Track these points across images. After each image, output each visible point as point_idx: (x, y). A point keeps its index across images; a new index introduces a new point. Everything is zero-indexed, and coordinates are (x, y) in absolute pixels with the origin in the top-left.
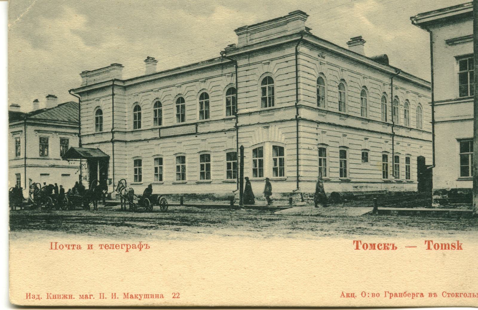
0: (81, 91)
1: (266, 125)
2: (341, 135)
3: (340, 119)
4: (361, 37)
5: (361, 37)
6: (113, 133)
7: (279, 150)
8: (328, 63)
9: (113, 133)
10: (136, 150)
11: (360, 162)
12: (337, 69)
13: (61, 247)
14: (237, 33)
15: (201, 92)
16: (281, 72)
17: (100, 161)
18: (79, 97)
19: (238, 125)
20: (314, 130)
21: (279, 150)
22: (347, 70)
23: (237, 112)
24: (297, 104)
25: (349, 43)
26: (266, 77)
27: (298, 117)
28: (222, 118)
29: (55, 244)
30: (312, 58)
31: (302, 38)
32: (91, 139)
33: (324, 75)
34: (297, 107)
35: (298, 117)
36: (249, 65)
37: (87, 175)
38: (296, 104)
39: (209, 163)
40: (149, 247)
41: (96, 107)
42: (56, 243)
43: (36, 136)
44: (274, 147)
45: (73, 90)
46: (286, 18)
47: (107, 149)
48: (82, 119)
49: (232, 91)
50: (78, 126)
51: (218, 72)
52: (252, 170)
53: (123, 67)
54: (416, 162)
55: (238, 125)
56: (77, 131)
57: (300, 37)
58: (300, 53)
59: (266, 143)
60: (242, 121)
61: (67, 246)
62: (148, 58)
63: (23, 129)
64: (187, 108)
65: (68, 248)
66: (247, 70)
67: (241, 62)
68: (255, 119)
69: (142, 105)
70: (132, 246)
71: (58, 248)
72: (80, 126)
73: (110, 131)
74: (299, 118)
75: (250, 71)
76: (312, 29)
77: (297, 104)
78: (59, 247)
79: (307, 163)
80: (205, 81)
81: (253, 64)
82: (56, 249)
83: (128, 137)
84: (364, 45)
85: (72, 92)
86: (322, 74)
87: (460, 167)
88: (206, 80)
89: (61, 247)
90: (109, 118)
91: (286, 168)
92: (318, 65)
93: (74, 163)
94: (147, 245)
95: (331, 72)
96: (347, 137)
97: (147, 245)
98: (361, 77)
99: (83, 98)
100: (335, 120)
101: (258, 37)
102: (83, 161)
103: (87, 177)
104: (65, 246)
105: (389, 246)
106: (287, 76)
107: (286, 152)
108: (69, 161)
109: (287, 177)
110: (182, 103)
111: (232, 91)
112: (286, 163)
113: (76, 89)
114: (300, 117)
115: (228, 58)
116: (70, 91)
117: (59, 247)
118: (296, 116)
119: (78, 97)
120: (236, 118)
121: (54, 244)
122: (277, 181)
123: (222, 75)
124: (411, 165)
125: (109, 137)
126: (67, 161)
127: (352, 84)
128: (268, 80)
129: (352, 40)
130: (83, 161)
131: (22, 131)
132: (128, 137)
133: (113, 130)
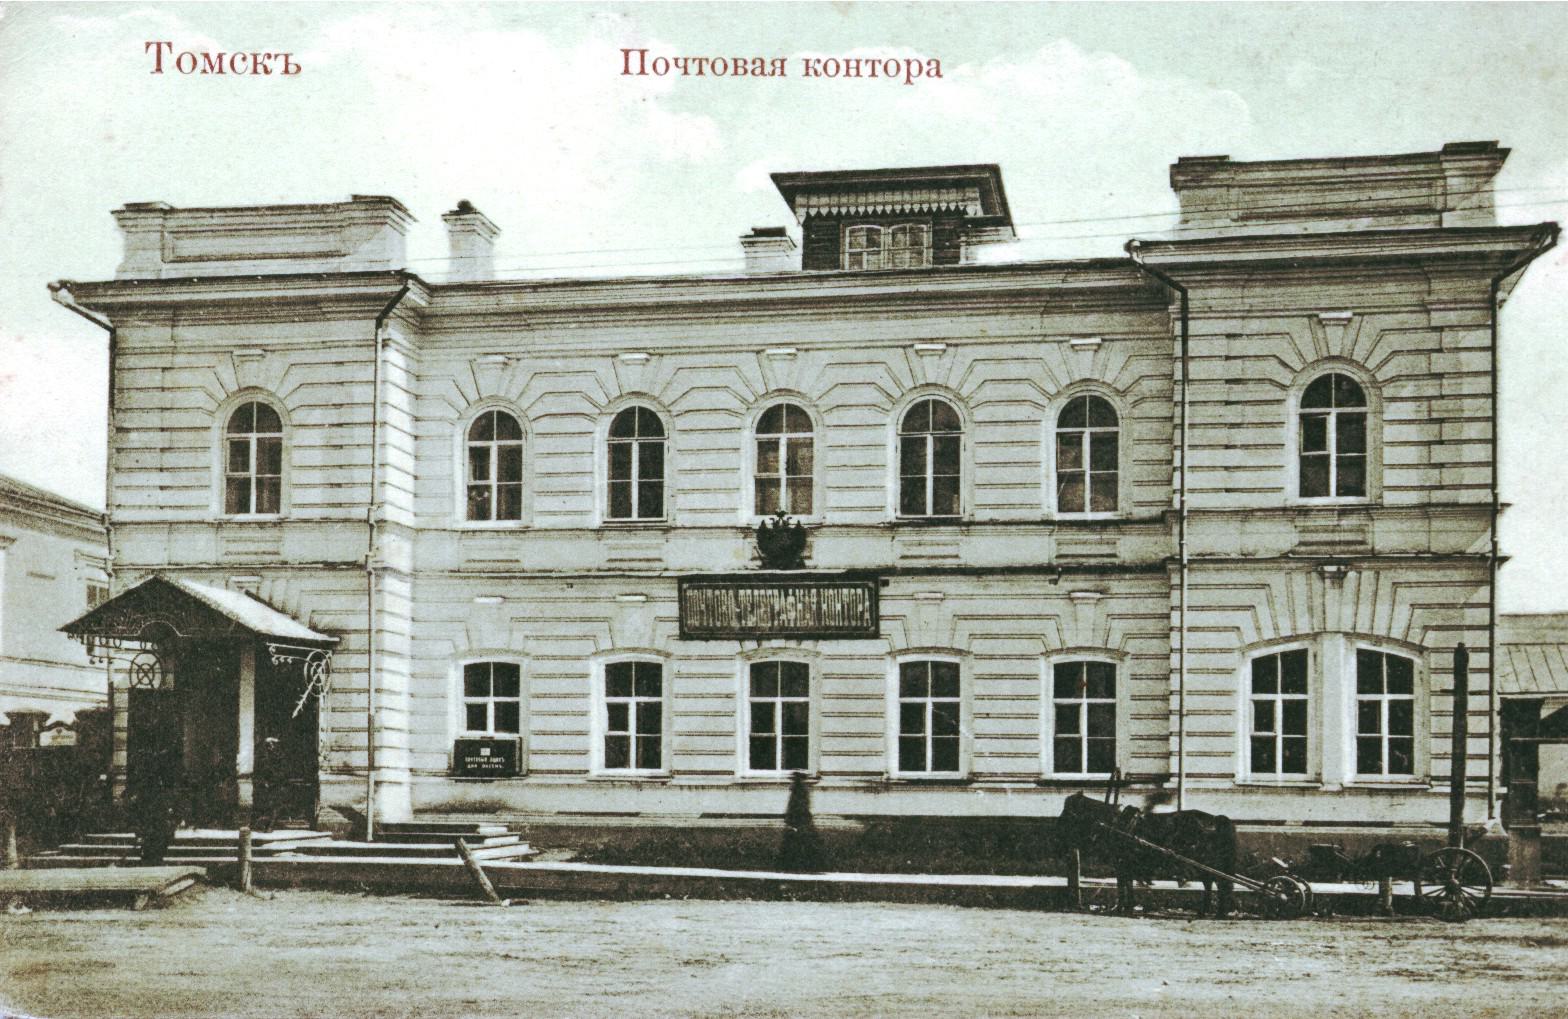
11: (526, 667)
13: (661, 67)
17: (162, 693)
29: (638, 55)
39: (1385, 690)
40: (299, 68)
42: (643, 52)
54: (1302, 647)
61: (681, 63)
65: (682, 70)
66: (1229, 336)
70: (926, 68)
71: (648, 68)
78: (838, 67)
82: (642, 72)
87: (1355, 742)
89: (661, 67)
94: (287, 56)
97: (287, 56)
104: (672, 63)
105: (269, 63)
117: (838, 67)
121: (635, 58)
123: (1044, 339)
124: (522, 700)
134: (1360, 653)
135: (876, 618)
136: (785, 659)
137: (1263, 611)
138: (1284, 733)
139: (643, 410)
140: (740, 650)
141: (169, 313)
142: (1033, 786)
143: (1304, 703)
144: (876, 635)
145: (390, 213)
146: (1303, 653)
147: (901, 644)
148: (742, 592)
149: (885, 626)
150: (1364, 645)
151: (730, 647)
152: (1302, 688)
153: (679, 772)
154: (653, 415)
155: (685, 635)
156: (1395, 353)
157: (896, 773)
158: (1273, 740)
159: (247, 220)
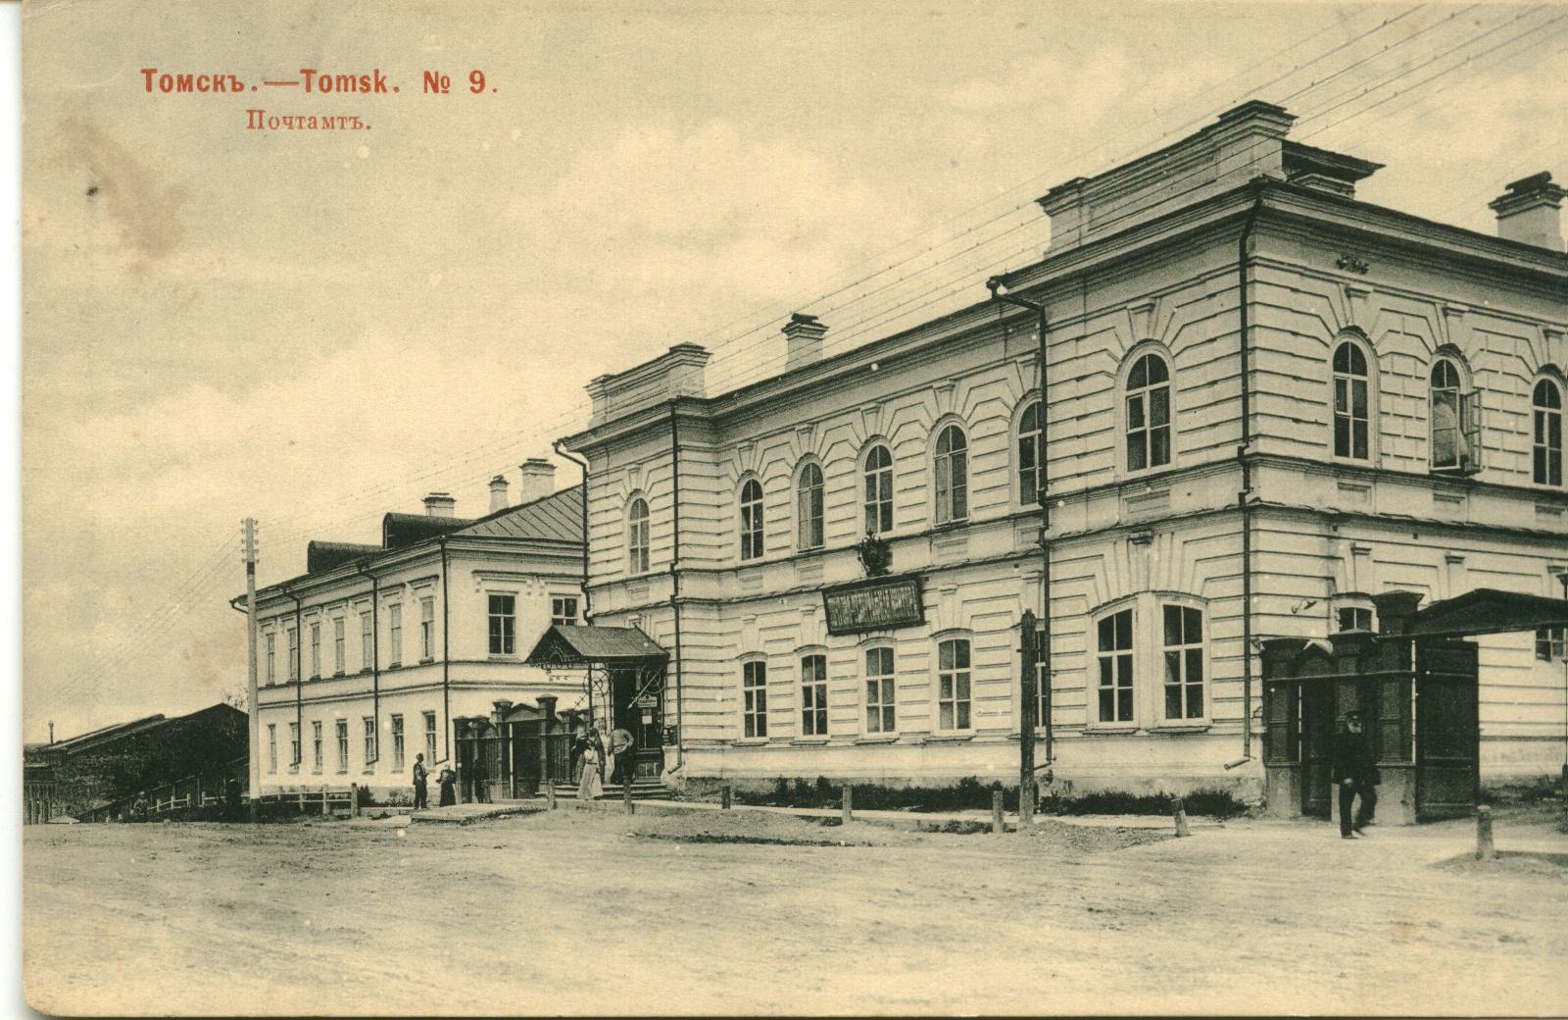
0: (593, 440)
1: (1142, 533)
2: (1437, 557)
3: (1435, 499)
4: (1547, 176)
5: (1547, 176)
6: (676, 574)
7: (1183, 623)
8: (1381, 290)
9: (676, 574)
10: (750, 634)
12: (1427, 309)
14: (1049, 208)
15: (941, 427)
16: (1191, 335)
18: (585, 461)
19: (1048, 534)
20: (1316, 545)
21: (1183, 623)
22: (1466, 308)
23: (1046, 490)
24: (1247, 452)
25: (1501, 206)
26: (1144, 358)
27: (1249, 498)
28: (1005, 511)
30: (1307, 273)
31: (1259, 203)
32: (620, 600)
33: (1364, 335)
34: (1246, 463)
35: (1249, 498)
36: (1085, 319)
37: (608, 716)
38: (1241, 450)
41: (631, 494)
43: (478, 591)
44: (1171, 613)
45: (565, 441)
46: (1211, 133)
47: (660, 629)
48: (593, 533)
49: (1035, 414)
50: (581, 554)
51: (994, 352)
52: (1163, 691)
53: (709, 354)
55: (1048, 534)
56: (580, 571)
57: (1250, 205)
58: (1258, 261)
59: (1140, 596)
60: (1066, 520)
62: (798, 318)
63: (440, 572)
64: (897, 485)
66: (1078, 339)
67: (1059, 312)
68: (1110, 511)
69: (764, 480)
72: (585, 555)
73: (667, 568)
74: (1254, 500)
75: (1089, 339)
76: (1381, 166)
77: (1247, 452)
79: (726, 681)
80: (953, 386)
81: (1102, 313)
83: (733, 588)
84: (1561, 203)
85: (562, 448)
86: (1355, 330)
88: (957, 384)
90: (666, 526)
91: (1210, 690)
92: (1335, 299)
93: (566, 677)
95: (1395, 322)
96: (1467, 564)
98: (1531, 332)
99: (601, 465)
100: (1420, 504)
101: (1120, 215)
102: (270, 675)
103: (608, 723)
106: (1206, 353)
107: (1209, 630)
108: (549, 670)
109: (1214, 721)
110: (882, 466)
111: (1035, 414)
112: (1209, 669)
113: (575, 437)
114: (1258, 499)
115: (1014, 299)
116: (556, 445)
118: (1242, 496)
119: (580, 463)
120: (1042, 515)
122: (1179, 734)
123: (1005, 362)
125: (662, 591)
126: (545, 671)
127: (1494, 362)
128: (1150, 370)
129: (1511, 191)
130: (270, 675)
131: (436, 577)
132: (733, 588)
133: (676, 568)
134: (1167, 608)
135: (922, 609)
136: (1187, 606)
137: (1100, 578)
138: (1188, 681)
139: (953, 427)
140: (858, 641)
141: (602, 450)
142: (1080, 735)
143: (1200, 651)
144: (922, 622)
145: (1256, 122)
146: (1129, 612)
147: (936, 629)
148: (852, 597)
149: (928, 615)
150: (1169, 601)
151: (853, 640)
152: (1129, 646)
153: (1222, 721)
154: (886, 449)
155: (834, 632)
156: (1184, 326)
157: (801, 737)
158: (1112, 691)
159: (667, 363)
